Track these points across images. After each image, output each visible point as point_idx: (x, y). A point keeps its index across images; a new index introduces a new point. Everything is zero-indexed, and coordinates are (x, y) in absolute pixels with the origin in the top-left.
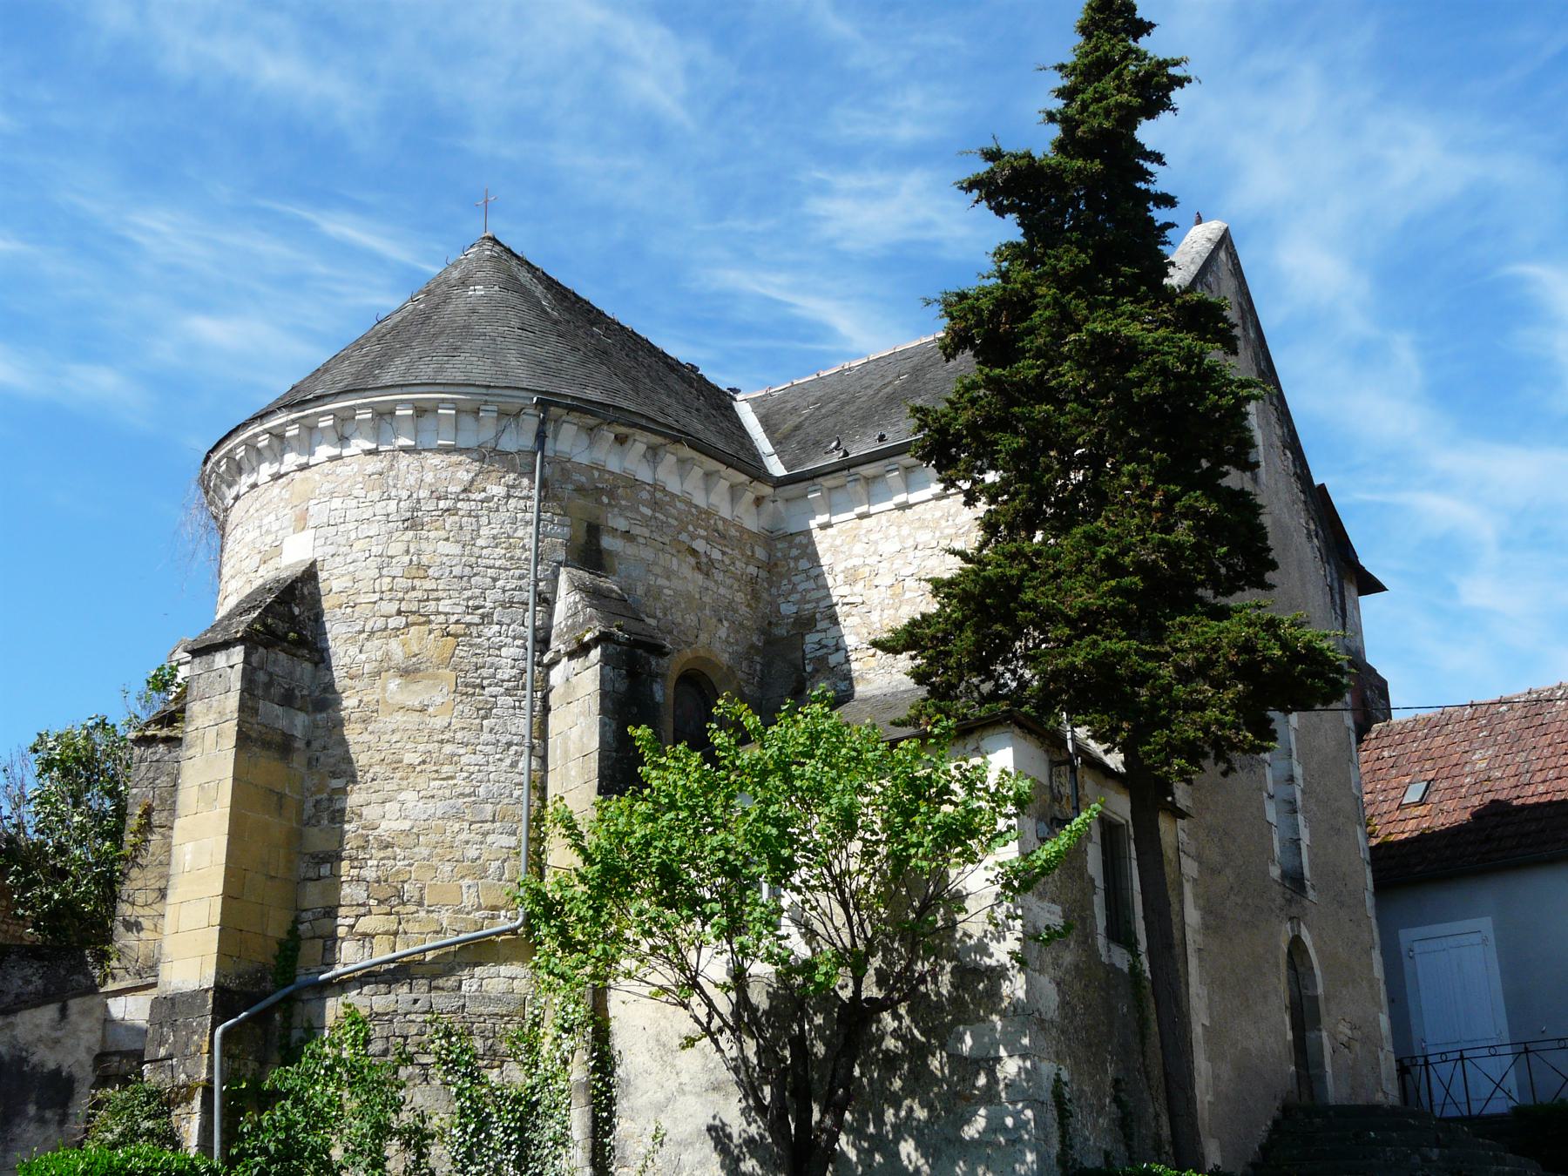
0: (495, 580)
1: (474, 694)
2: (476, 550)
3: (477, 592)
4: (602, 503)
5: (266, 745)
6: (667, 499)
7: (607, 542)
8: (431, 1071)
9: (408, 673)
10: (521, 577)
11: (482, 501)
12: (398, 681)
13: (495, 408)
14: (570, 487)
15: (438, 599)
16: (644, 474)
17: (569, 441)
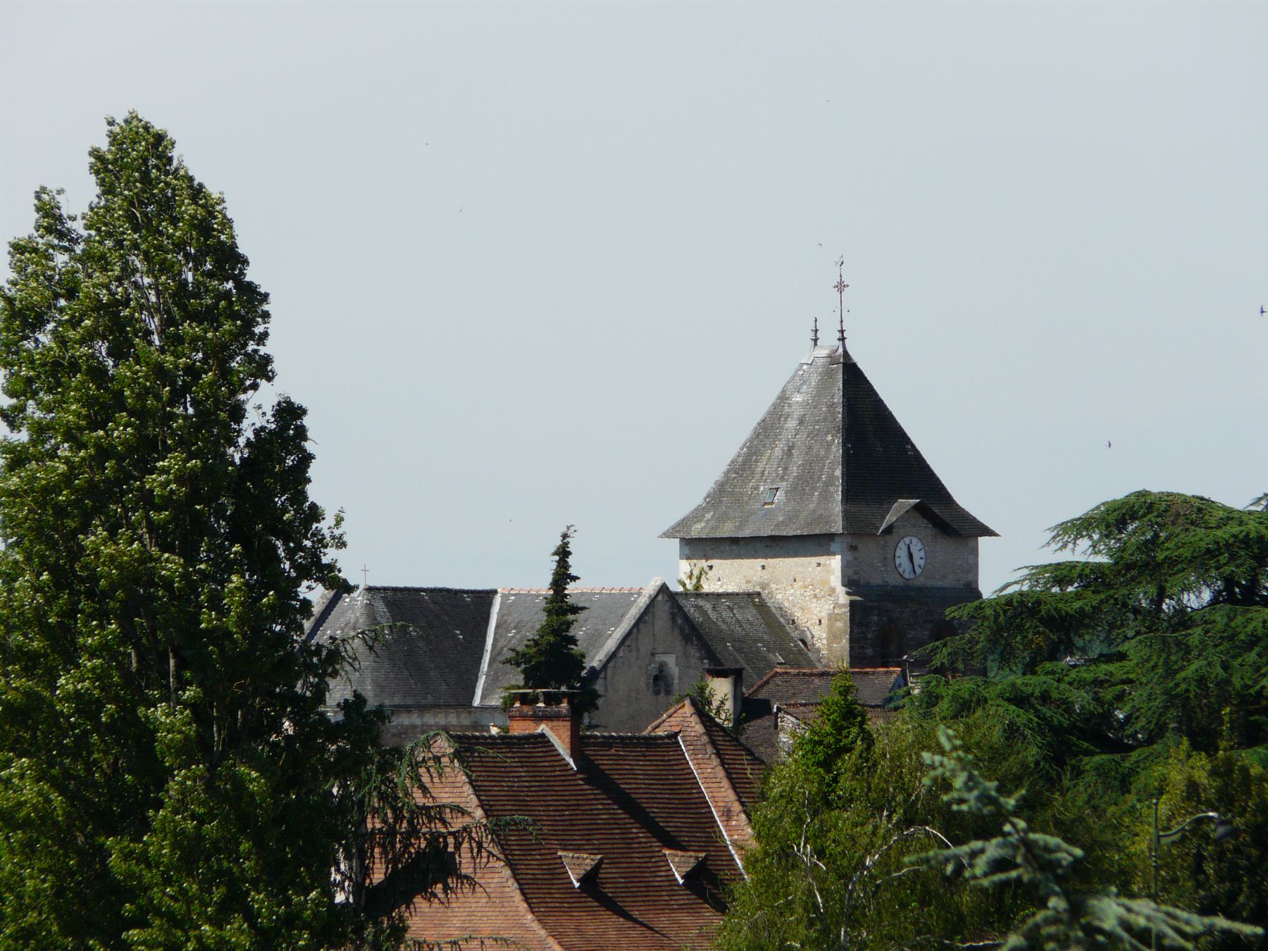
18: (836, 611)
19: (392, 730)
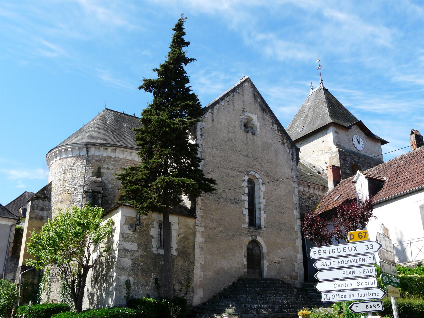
0: (77, 182)
1: (72, 205)
2: (74, 176)
3: (74, 184)
4: (102, 163)
5: (36, 218)
6: (119, 159)
7: (102, 171)
8: (59, 280)
9: (61, 202)
10: (82, 181)
11: (76, 166)
12: (60, 204)
13: (78, 147)
14: (94, 161)
15: (67, 187)
16: (112, 155)
17: (93, 151)
18: (332, 156)
19: (96, 158)
